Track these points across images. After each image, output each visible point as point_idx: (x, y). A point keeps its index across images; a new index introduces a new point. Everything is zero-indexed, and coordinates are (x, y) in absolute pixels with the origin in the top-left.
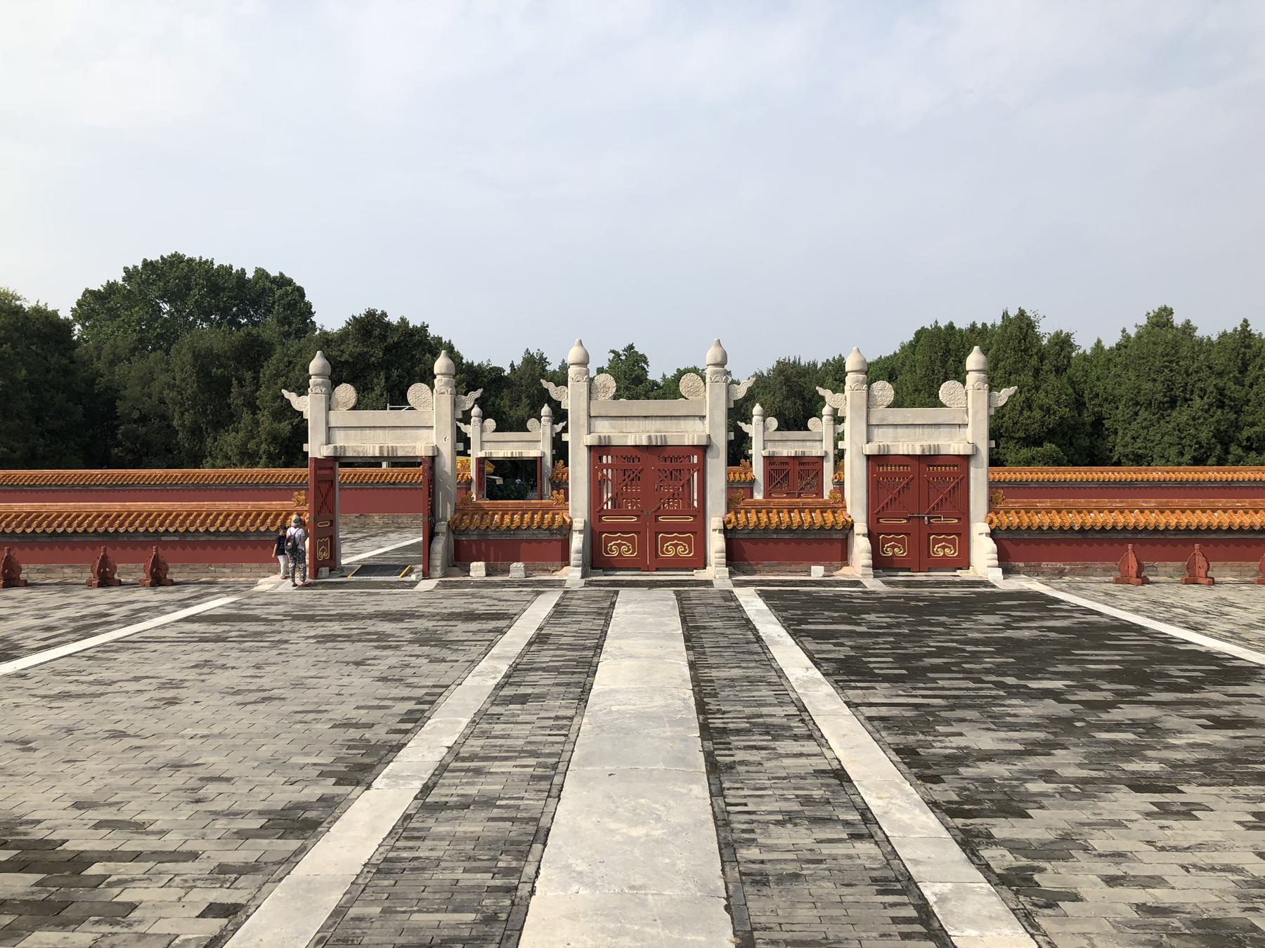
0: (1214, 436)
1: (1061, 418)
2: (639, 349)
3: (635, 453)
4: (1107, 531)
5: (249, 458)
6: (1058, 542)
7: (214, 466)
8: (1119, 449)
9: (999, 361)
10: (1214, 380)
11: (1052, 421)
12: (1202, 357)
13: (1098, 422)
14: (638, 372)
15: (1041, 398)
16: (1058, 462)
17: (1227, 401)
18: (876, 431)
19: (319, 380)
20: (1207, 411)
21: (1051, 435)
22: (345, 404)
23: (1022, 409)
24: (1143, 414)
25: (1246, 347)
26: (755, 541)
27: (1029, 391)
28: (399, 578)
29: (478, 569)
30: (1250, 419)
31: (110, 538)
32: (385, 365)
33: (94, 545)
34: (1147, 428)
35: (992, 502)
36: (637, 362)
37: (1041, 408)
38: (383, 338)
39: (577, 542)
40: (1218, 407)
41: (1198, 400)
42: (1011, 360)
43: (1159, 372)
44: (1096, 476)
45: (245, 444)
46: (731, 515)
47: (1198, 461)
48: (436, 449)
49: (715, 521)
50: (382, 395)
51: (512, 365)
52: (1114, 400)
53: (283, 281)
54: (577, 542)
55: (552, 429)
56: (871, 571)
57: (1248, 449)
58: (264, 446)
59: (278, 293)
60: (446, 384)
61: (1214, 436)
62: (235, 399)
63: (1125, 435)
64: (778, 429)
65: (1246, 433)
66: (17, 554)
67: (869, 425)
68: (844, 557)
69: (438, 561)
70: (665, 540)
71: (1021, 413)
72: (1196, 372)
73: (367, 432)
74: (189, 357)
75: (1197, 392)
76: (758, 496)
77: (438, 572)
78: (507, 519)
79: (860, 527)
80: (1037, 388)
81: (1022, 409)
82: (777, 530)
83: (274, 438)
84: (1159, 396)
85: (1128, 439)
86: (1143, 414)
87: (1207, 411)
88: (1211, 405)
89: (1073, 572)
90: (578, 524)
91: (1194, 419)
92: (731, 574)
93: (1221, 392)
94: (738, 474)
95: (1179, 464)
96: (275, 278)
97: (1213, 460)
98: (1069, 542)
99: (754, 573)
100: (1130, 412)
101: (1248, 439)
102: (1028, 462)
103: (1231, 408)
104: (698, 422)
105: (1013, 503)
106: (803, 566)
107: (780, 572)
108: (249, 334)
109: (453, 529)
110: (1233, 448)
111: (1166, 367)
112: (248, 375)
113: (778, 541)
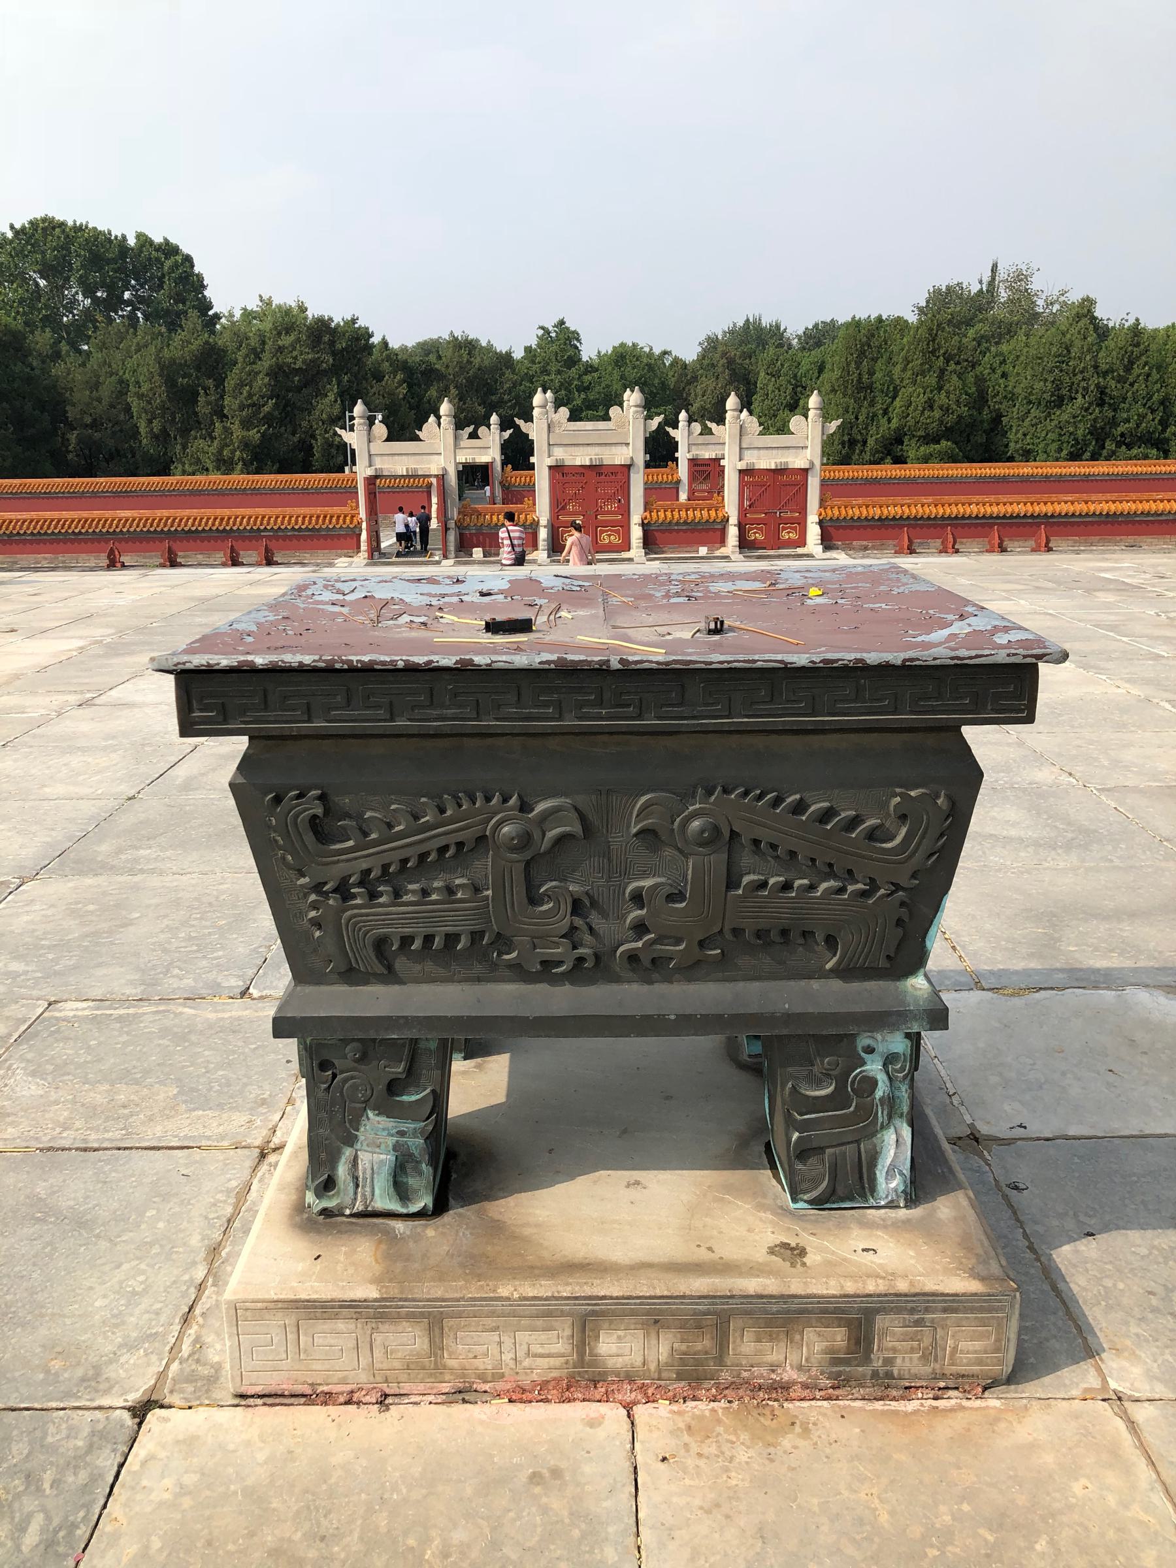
0: (1091, 433)
2: (571, 325)
3: (583, 471)
5: (225, 465)
6: (865, 527)
7: (184, 473)
8: (1012, 445)
9: (909, 363)
11: (951, 419)
12: (1088, 358)
13: (997, 419)
14: (571, 353)
15: (942, 399)
17: (1107, 399)
18: (747, 454)
19: (362, 421)
20: (1087, 410)
22: (380, 438)
23: (924, 409)
24: (1034, 412)
25: (1135, 346)
26: (663, 531)
27: (932, 391)
28: (427, 559)
29: (478, 553)
31: (172, 535)
32: (336, 371)
33: (161, 540)
34: (1036, 424)
35: (822, 502)
36: (569, 339)
38: (332, 343)
39: (543, 534)
40: (1098, 405)
41: (1080, 399)
42: (919, 362)
43: (1051, 371)
44: (1106, 470)
45: (220, 452)
46: (647, 514)
47: (1074, 457)
48: (444, 469)
49: (636, 518)
50: (336, 401)
52: (1012, 398)
53: (169, 249)
54: (543, 534)
55: (501, 436)
56: (737, 549)
57: (1119, 445)
58: (238, 453)
59: (168, 264)
60: (449, 422)
61: (1091, 433)
62: (203, 407)
63: (1017, 431)
64: (701, 434)
65: (1120, 429)
66: (176, 546)
67: (741, 449)
68: (723, 541)
69: (452, 547)
70: (602, 532)
71: (923, 412)
72: (1082, 372)
73: (396, 457)
74: (155, 369)
75: (1081, 390)
76: (683, 497)
77: (453, 554)
78: (495, 518)
79: (733, 520)
80: (940, 388)
81: (924, 409)
82: (677, 524)
83: (246, 445)
84: (1047, 396)
85: (1020, 435)
86: (1034, 412)
87: (1087, 410)
88: (1091, 404)
89: (874, 548)
90: (544, 521)
91: (1074, 417)
92: (646, 554)
93: (1102, 391)
94: (661, 475)
95: (1057, 460)
96: (160, 245)
98: (872, 527)
99: (663, 552)
100: (1024, 409)
101: (1122, 435)
102: (926, 460)
103: (1110, 405)
104: (625, 447)
105: (837, 501)
106: (694, 548)
107: (679, 552)
108: (207, 343)
109: (459, 526)
110: (1110, 445)
111: (1057, 367)
112: (210, 383)
113: (678, 531)
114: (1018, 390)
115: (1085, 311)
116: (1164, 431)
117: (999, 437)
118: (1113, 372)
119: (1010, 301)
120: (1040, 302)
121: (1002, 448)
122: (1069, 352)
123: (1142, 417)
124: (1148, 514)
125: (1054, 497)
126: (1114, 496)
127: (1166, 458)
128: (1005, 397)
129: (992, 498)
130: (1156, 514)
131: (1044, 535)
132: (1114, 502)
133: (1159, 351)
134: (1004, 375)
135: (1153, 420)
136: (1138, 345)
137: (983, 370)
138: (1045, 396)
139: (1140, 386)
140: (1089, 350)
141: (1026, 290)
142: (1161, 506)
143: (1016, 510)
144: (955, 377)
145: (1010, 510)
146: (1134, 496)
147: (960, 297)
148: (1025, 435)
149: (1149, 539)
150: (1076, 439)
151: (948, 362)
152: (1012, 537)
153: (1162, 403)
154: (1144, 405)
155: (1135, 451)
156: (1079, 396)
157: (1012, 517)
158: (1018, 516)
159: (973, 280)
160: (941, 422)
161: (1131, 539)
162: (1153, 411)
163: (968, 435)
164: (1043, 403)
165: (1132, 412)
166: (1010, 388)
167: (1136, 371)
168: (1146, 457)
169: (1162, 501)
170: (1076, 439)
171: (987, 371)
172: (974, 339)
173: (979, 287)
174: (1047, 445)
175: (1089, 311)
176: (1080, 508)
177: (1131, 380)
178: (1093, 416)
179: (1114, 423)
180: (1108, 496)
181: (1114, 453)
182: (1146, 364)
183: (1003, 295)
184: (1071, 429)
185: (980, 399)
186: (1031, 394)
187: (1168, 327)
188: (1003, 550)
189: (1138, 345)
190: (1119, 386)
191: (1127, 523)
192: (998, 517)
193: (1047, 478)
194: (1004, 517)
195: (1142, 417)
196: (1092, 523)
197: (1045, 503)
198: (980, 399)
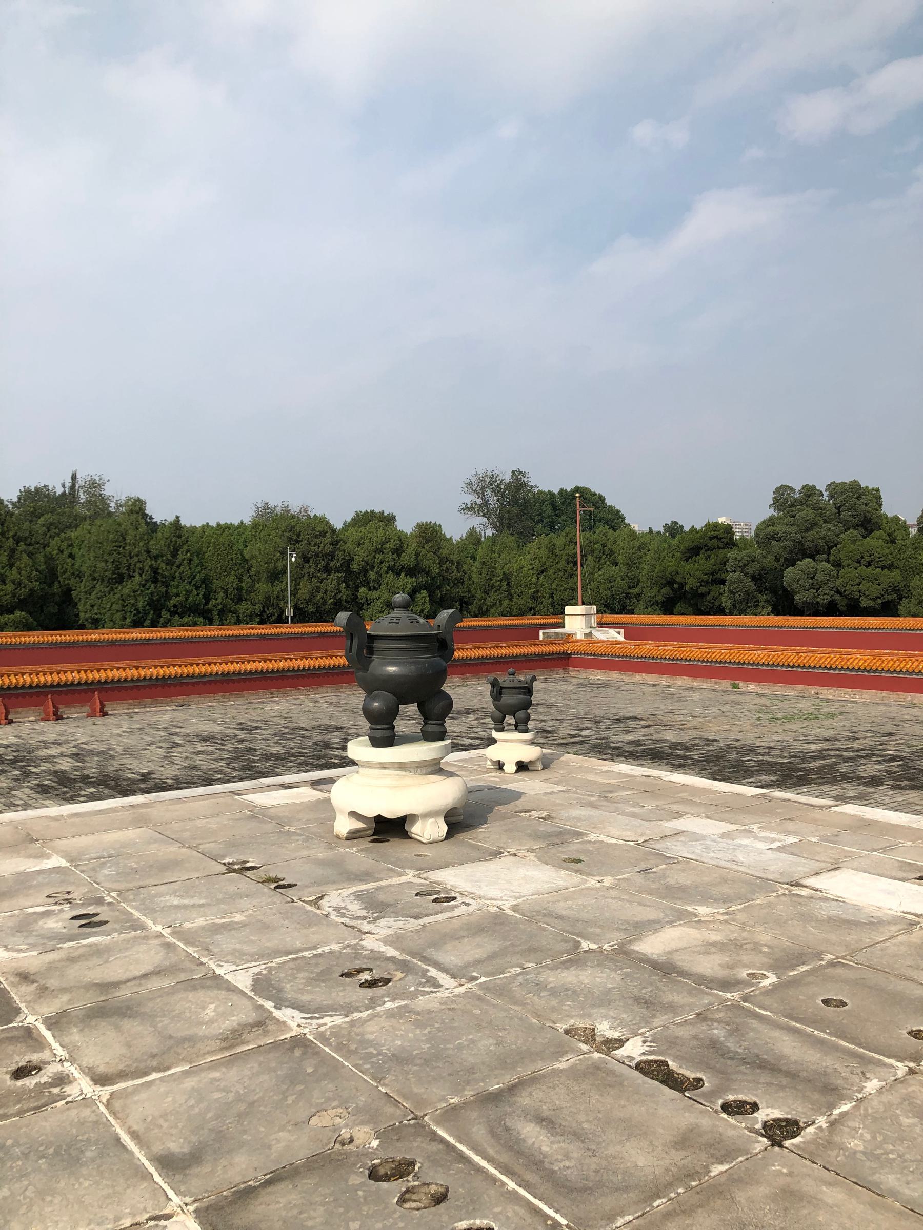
1: (31, 590)
4: (47, 687)
8: (82, 615)
10: (149, 562)
11: (23, 592)
12: (141, 544)
16: (28, 628)
20: (144, 586)
21: (22, 604)
24: (99, 587)
30: (175, 591)
37: (13, 582)
40: (153, 582)
43: (110, 554)
44: (163, 635)
47: (137, 624)
51: (468, 509)
52: (79, 576)
63: (85, 603)
72: (137, 555)
75: (137, 570)
80: (11, 566)
84: (109, 574)
85: (88, 607)
86: (99, 587)
87: (144, 586)
88: (147, 581)
91: (134, 592)
93: (155, 571)
95: (122, 627)
97: (148, 622)
100: (90, 584)
101: (175, 606)
103: (163, 582)
110: (165, 615)
111: (115, 551)
114: (84, 569)
115: (137, 508)
116: (207, 603)
117: (70, 608)
118: (162, 556)
119: (88, 502)
120: (112, 505)
121: (73, 618)
122: (124, 539)
123: (189, 592)
124: (193, 676)
125: (106, 665)
126: (162, 661)
127: (210, 625)
128: (73, 574)
129: (46, 668)
130: (199, 676)
131: (98, 701)
132: (162, 667)
133: (198, 542)
134: (71, 556)
135: (198, 595)
136: (180, 536)
137: (53, 549)
138: (107, 573)
139: (185, 568)
140: (141, 539)
141: (101, 495)
142: (203, 669)
143: (70, 678)
144: (25, 556)
145: (63, 678)
146: (179, 661)
147: (48, 496)
148: (92, 606)
149: (196, 699)
150: (137, 609)
151: (18, 543)
152: (68, 704)
153: (203, 581)
154: (190, 583)
155: (186, 619)
156: (136, 574)
157: (66, 685)
158: (72, 684)
159: (57, 483)
160: (14, 595)
161: (180, 700)
162: (197, 588)
163: (41, 607)
164: (106, 580)
165: (180, 589)
166: (76, 567)
167: (180, 557)
168: (195, 624)
169: (204, 664)
170: (137, 609)
171: (55, 552)
172: (44, 525)
173: (62, 490)
174: (113, 615)
175: (141, 509)
176: (132, 673)
177: (177, 563)
178: (149, 591)
179: (167, 596)
180: (157, 662)
181: (169, 620)
182: (188, 551)
183: (83, 497)
184: (132, 601)
185: (51, 575)
186: (94, 572)
187: (203, 526)
188: (58, 717)
189: (180, 536)
190: (168, 568)
191: (175, 685)
192: (52, 686)
193: (113, 643)
194: (59, 685)
195: (189, 592)
196: (144, 687)
197: (98, 671)
198: (51, 575)
